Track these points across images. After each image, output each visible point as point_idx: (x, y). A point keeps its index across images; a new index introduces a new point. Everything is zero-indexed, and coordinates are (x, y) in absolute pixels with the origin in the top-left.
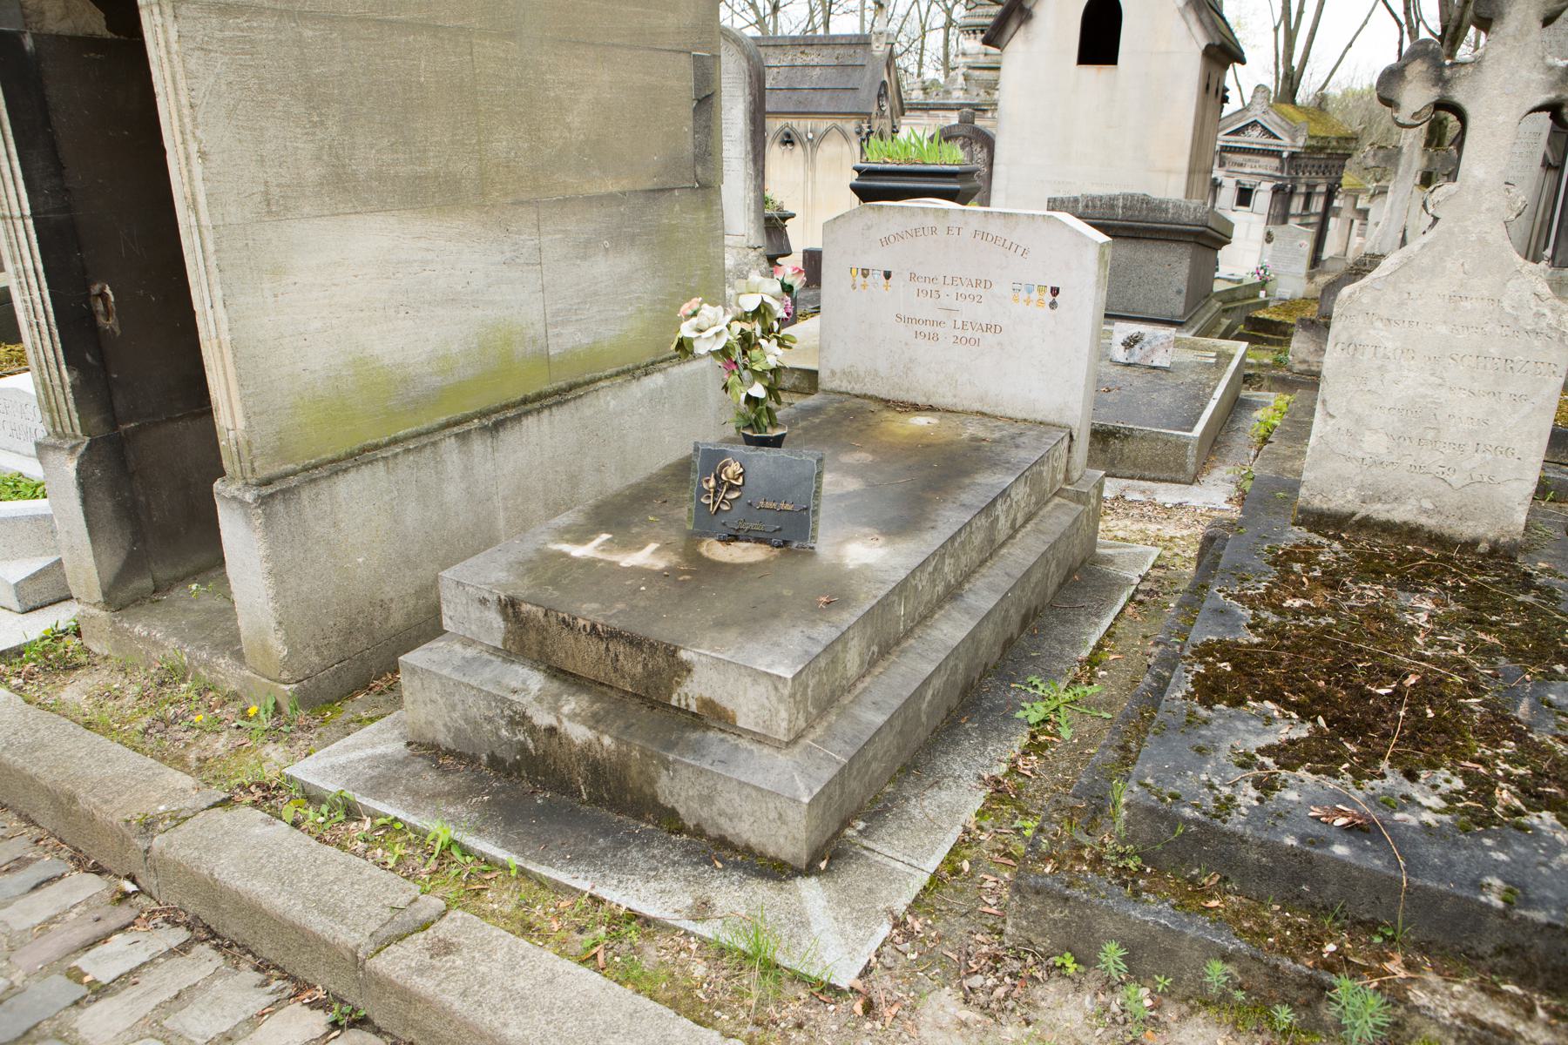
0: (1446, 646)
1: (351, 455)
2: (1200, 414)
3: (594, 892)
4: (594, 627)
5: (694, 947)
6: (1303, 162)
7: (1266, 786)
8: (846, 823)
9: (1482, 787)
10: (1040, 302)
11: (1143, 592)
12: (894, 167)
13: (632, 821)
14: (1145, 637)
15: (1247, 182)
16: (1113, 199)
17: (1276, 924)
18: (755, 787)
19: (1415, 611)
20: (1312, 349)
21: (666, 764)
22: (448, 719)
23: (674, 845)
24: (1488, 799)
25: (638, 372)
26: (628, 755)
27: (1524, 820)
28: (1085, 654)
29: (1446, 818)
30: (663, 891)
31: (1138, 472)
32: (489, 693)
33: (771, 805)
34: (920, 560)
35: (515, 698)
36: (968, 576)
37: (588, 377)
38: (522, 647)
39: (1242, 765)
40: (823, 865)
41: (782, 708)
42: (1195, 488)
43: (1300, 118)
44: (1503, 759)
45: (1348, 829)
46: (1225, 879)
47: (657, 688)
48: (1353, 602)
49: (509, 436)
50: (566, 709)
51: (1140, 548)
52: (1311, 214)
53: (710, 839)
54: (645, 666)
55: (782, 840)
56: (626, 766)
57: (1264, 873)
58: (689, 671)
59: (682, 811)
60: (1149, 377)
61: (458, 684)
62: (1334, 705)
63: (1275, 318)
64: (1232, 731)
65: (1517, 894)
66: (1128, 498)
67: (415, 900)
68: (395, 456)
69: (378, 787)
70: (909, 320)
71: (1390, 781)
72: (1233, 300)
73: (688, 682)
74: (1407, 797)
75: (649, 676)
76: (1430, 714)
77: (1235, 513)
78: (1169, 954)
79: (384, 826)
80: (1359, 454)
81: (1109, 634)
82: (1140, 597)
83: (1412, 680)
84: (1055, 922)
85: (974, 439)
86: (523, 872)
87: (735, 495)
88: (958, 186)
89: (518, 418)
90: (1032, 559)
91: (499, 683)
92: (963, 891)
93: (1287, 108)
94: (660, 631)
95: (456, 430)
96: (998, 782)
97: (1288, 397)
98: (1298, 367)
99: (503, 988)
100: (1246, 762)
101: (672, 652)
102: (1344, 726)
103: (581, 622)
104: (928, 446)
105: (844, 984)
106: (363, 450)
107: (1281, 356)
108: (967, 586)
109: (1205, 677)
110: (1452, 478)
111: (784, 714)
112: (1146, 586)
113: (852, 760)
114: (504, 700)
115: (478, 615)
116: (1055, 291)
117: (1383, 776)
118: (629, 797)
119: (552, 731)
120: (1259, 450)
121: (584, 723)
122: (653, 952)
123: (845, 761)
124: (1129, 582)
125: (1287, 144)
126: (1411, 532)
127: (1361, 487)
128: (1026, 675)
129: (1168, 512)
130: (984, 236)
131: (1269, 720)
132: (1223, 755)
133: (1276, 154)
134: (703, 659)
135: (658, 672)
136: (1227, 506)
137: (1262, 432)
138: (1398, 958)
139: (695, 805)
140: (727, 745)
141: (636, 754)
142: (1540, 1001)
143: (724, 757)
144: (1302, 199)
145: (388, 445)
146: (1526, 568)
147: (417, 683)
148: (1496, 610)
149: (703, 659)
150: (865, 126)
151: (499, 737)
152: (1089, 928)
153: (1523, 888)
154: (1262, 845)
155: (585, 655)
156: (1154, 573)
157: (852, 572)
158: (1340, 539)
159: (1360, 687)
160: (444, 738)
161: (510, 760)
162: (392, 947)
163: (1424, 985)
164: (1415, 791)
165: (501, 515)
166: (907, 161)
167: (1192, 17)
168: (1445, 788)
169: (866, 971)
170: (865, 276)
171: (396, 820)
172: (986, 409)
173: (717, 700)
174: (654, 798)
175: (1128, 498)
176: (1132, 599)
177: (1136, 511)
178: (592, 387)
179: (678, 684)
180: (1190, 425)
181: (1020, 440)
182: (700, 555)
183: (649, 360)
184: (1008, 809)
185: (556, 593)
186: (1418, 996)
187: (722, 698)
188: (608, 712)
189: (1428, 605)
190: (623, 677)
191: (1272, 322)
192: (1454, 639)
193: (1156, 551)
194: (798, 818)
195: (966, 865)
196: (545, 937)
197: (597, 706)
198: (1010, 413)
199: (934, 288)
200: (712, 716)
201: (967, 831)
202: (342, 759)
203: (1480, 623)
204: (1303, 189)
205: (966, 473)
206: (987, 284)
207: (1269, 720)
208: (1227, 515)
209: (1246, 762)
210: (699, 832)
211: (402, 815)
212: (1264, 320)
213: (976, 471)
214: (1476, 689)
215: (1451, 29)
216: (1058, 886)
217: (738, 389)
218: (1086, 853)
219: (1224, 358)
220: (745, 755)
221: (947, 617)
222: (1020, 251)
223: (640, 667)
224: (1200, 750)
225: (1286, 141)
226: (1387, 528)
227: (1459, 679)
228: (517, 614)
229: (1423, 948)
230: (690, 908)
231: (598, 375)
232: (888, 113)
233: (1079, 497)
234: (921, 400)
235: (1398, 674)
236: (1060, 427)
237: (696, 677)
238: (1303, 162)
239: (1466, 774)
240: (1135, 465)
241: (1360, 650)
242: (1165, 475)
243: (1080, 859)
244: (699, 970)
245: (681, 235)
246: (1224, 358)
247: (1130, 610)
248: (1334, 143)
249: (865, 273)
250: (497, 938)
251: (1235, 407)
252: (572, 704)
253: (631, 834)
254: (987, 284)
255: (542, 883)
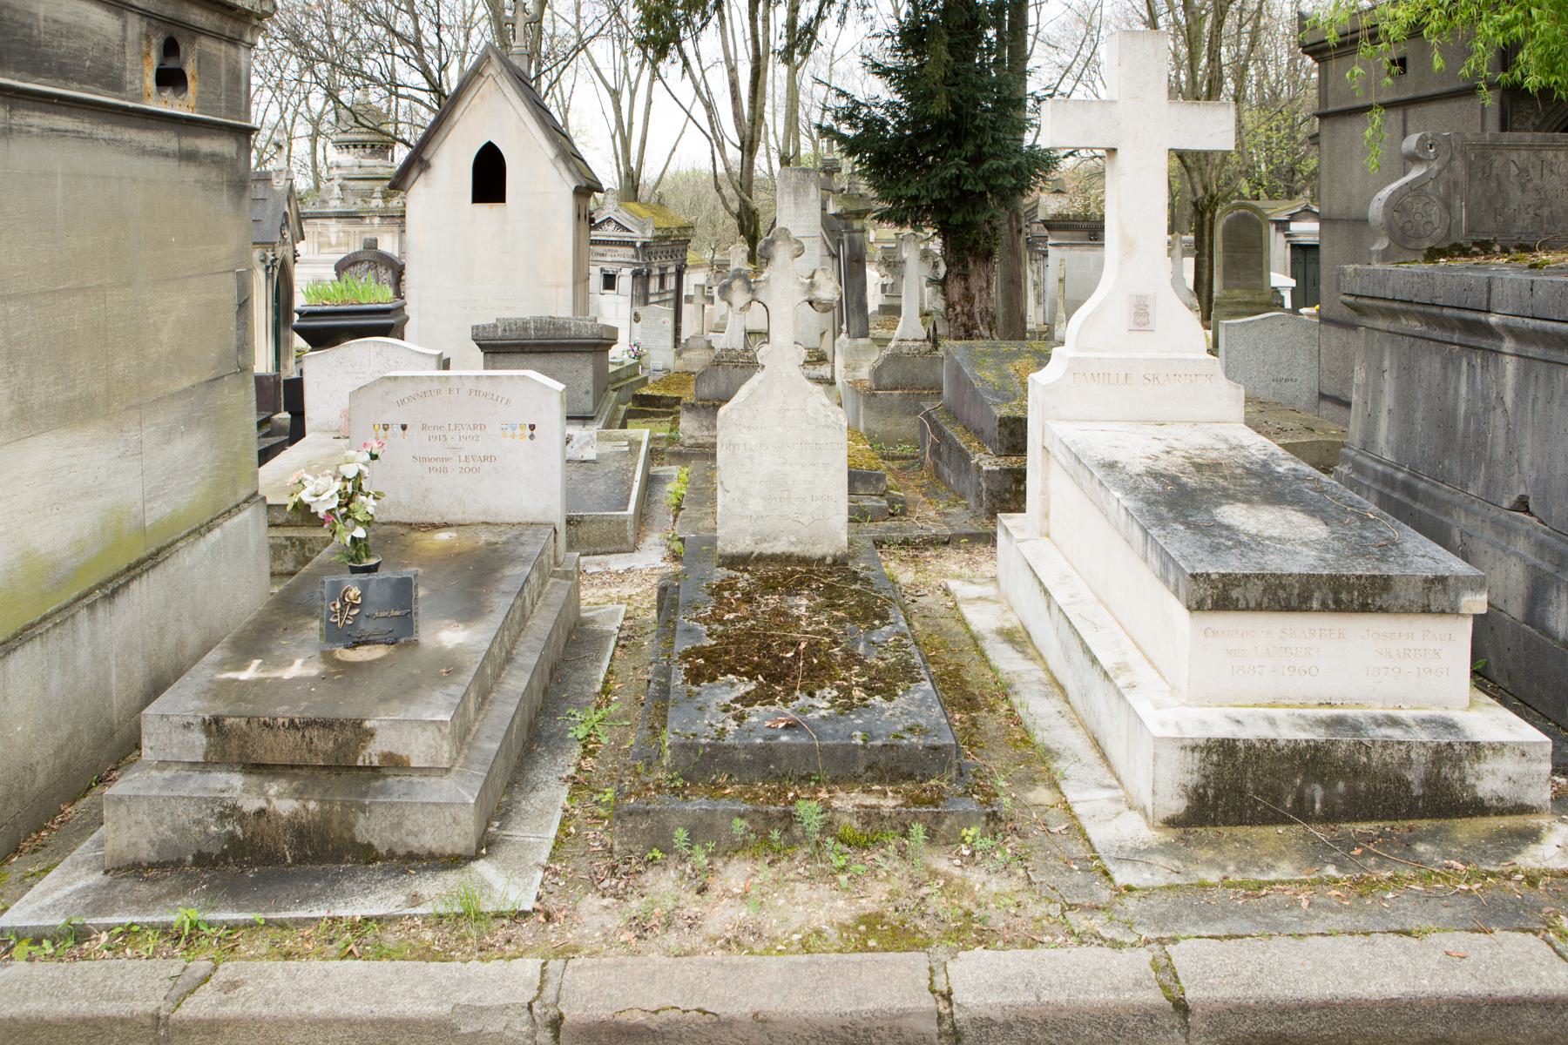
0: (818, 623)
1: (15, 636)
2: (629, 495)
3: (331, 915)
4: (292, 721)
5: (419, 923)
6: (653, 250)
7: (740, 718)
8: (488, 825)
9: (846, 692)
10: (522, 436)
11: (624, 638)
12: (333, 308)
13: (334, 866)
14: (635, 669)
15: (610, 269)
16: (525, 323)
17: (761, 792)
18: (435, 804)
19: (798, 606)
20: (696, 426)
21: (363, 809)
22: (153, 835)
23: (373, 870)
24: (849, 696)
25: (203, 530)
26: (330, 812)
27: (867, 702)
28: (598, 688)
29: (832, 711)
30: (381, 899)
31: (592, 550)
32: (200, 798)
33: (447, 814)
34: (494, 634)
35: (225, 795)
36: (514, 643)
37: (169, 540)
38: (224, 755)
39: (725, 711)
40: (484, 851)
41: (444, 743)
42: (636, 554)
43: (645, 213)
44: (855, 675)
45: (787, 727)
46: (730, 776)
47: (345, 756)
48: (763, 608)
49: (121, 601)
50: (272, 792)
51: (610, 607)
52: (667, 292)
53: (400, 858)
54: (336, 740)
55: (456, 838)
56: (328, 821)
57: (750, 765)
58: (372, 735)
59: (376, 843)
60: (583, 470)
61: (167, 800)
62: (765, 668)
63: (657, 393)
64: (714, 695)
65: (869, 736)
66: (589, 571)
67: (185, 968)
68: (48, 630)
69: (98, 907)
70: (424, 459)
71: (802, 700)
72: (619, 380)
73: (372, 744)
74: (812, 706)
75: (339, 748)
76: (815, 661)
77: (673, 567)
78: (711, 826)
79: (121, 933)
80: (748, 513)
81: (610, 672)
82: (622, 642)
83: (803, 646)
84: (644, 830)
85: (489, 544)
86: (268, 923)
87: (355, 612)
88: (392, 321)
89: (127, 584)
90: (550, 625)
91: (206, 788)
92: (576, 845)
93: (633, 206)
94: (346, 711)
95: (85, 601)
96: (574, 778)
97: (686, 470)
98: (689, 442)
99: (293, 991)
100: (726, 709)
101: (357, 724)
102: (773, 678)
103: (280, 721)
104: (458, 554)
105: (528, 908)
106: (24, 630)
107: (673, 434)
108: (514, 652)
109: (691, 669)
110: (803, 520)
111: (446, 748)
112: (624, 634)
113: (489, 773)
114: (214, 800)
115: (181, 738)
116: (532, 427)
117: (798, 698)
118: (330, 847)
119: (261, 812)
120: (676, 517)
121: (291, 797)
122: (391, 936)
123: (485, 775)
124: (611, 633)
125: (639, 235)
126: (787, 559)
127: (753, 535)
128: (564, 710)
129: (621, 577)
130: (477, 392)
131: (733, 685)
132: (713, 708)
133: (631, 244)
134: (384, 723)
135: (347, 743)
136: (663, 564)
137: (675, 501)
138: (824, 790)
139: (387, 834)
140: (404, 784)
141: (338, 808)
142: (888, 789)
143: (406, 791)
144: (658, 280)
145: (40, 622)
146: (854, 568)
147: (123, 810)
148: (841, 596)
149: (384, 723)
150: (269, 254)
151: (207, 834)
152: (664, 827)
153: (870, 732)
154: (746, 748)
155: (283, 747)
156: (627, 623)
157: (452, 650)
158: (747, 571)
159: (777, 656)
160: (146, 853)
161: (216, 851)
162: (188, 999)
163: (838, 798)
164: (814, 702)
165: (114, 671)
166: (344, 302)
167: (562, 166)
168: (829, 697)
169: (539, 899)
170: (385, 429)
171: (132, 924)
172: (489, 519)
173: (394, 751)
174: (353, 839)
175: (589, 571)
176: (617, 645)
177: (596, 581)
178: (173, 549)
179: (363, 747)
180: (624, 505)
181: (524, 539)
182: (338, 660)
183: (209, 518)
184: (586, 793)
185: (250, 706)
186: (836, 803)
187: (399, 749)
188: (306, 786)
189: (805, 602)
190: (317, 755)
191: (655, 397)
192: (822, 618)
193: (623, 608)
194: (467, 816)
195: (573, 830)
196: (307, 955)
197: (295, 784)
198: (508, 520)
199: (441, 433)
200: (395, 764)
201: (566, 810)
202: (48, 901)
203: (834, 606)
204: (656, 272)
205: (494, 570)
206: (482, 427)
207: (733, 685)
208: (664, 571)
209: (726, 709)
210: (391, 855)
211: (137, 919)
212: (648, 396)
213: (502, 567)
214: (836, 642)
215: (747, 143)
216: (641, 806)
217: (344, 534)
218: (651, 786)
219: (634, 444)
220: (419, 787)
221: (510, 674)
222: (504, 401)
223: (331, 744)
224: (700, 709)
225: (637, 233)
226: (774, 558)
227: (827, 640)
228: (220, 730)
229: (834, 782)
230: (407, 901)
231: (176, 537)
232: (289, 240)
233: (567, 575)
234: (437, 520)
235: (795, 644)
236: (547, 525)
237: (377, 738)
238: (653, 250)
239: (838, 687)
240: (588, 544)
241: (773, 636)
242: (612, 548)
243: (649, 789)
244: (428, 935)
245: (228, 411)
246: (634, 444)
247: (618, 653)
248: (676, 232)
249: (386, 428)
250: (270, 966)
251: (650, 481)
252: (273, 788)
253: (337, 874)
254: (482, 427)
255: (282, 925)
